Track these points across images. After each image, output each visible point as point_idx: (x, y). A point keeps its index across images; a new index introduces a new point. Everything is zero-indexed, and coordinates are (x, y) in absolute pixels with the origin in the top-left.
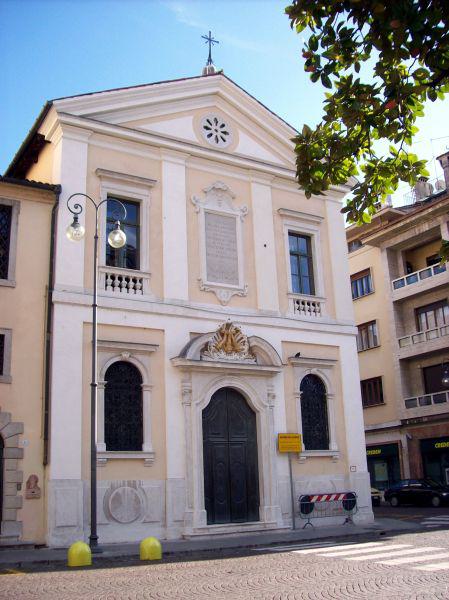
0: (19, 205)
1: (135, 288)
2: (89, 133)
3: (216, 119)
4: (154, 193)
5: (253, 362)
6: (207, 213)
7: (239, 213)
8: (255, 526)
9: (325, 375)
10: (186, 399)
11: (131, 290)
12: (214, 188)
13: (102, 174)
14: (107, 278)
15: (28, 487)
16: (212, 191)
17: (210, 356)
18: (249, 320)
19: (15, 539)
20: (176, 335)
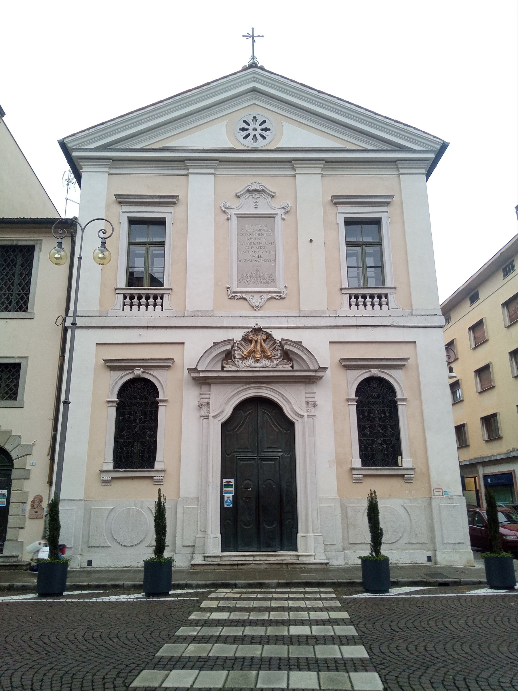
0: (41, 244)
1: (380, 304)
2: (109, 163)
3: (255, 118)
4: (178, 210)
5: (288, 367)
6: (240, 217)
7: (280, 212)
8: (285, 556)
9: (396, 378)
10: (203, 412)
11: (377, 307)
12: (248, 191)
13: (123, 200)
14: (350, 298)
15: (33, 507)
16: (248, 195)
17: (235, 365)
18: (284, 322)
19: (14, 559)
20: (195, 348)
